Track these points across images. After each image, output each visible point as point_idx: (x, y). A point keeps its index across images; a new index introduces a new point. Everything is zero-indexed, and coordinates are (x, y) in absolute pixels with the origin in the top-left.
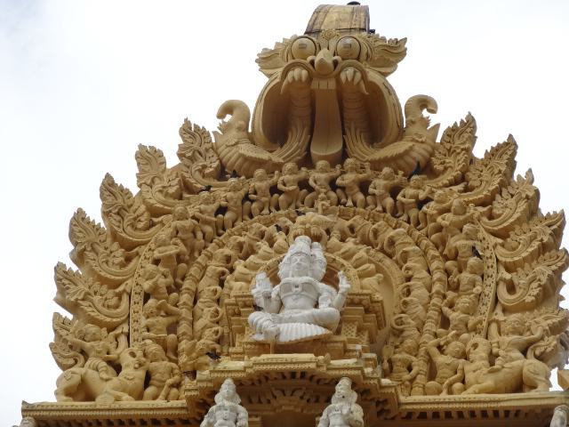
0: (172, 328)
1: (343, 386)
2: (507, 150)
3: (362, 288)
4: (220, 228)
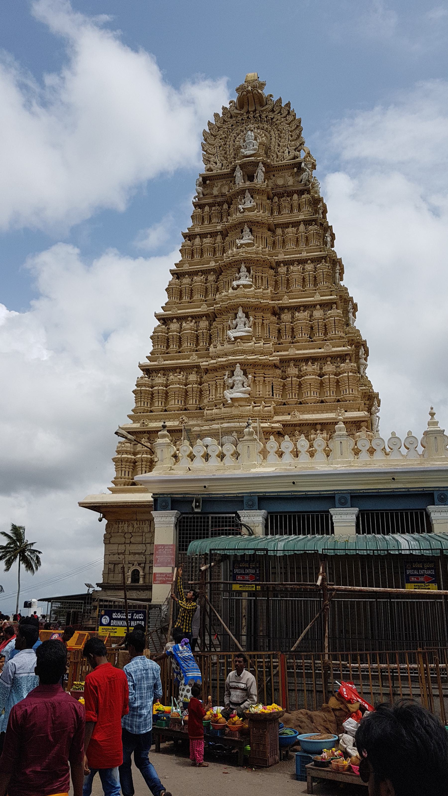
0: (226, 153)
1: (261, 164)
4: (233, 130)
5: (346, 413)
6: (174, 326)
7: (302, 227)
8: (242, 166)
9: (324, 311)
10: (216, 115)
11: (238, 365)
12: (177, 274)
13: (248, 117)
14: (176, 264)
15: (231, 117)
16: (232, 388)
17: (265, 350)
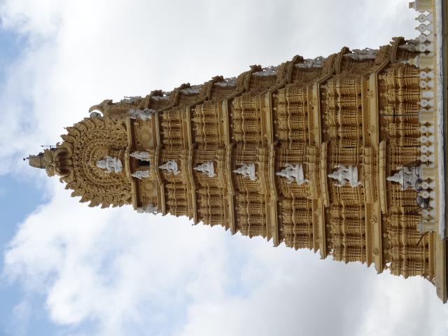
0: (113, 186)
1: (132, 155)
2: (68, 129)
3: (154, 148)
4: (88, 180)
5: (370, 90)
6: (203, 211)
7: (195, 120)
8: (132, 171)
9: (278, 103)
10: (73, 195)
11: (329, 176)
12: (235, 229)
13: (78, 166)
14: (363, 263)
15: (76, 181)
16: (348, 181)
17: (186, 155)
